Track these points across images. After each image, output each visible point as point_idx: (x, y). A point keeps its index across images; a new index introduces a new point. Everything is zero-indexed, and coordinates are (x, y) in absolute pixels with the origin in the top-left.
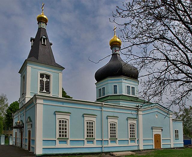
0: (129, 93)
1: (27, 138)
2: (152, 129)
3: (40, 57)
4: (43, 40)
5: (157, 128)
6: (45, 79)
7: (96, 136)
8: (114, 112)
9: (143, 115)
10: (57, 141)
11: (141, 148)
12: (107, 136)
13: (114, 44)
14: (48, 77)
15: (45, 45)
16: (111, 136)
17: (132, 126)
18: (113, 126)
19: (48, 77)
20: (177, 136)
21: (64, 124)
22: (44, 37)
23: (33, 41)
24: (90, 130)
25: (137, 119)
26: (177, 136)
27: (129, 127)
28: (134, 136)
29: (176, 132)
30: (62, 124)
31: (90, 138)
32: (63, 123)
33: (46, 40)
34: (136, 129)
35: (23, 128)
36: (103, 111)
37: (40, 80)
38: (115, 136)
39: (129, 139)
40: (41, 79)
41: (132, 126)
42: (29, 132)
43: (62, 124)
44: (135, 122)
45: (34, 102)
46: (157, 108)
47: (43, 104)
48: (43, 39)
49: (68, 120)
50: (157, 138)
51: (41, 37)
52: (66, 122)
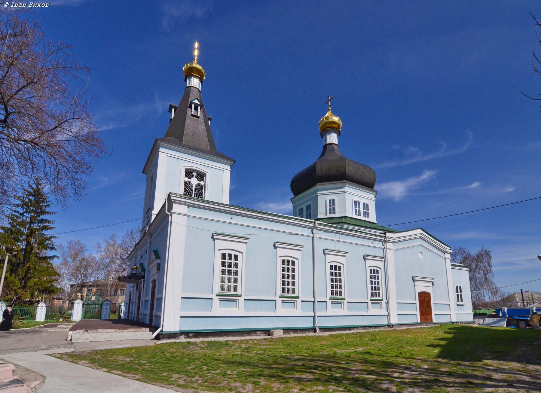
0: (357, 212)
1: (149, 298)
2: (414, 281)
3: (186, 140)
4: (193, 107)
5: (424, 280)
6: (194, 181)
7: (302, 288)
8: (339, 241)
9: (394, 250)
10: (216, 300)
11: (394, 320)
12: (324, 291)
13: (328, 126)
14: (201, 176)
15: (198, 117)
16: (332, 293)
17: (374, 272)
18: (336, 269)
19: (201, 176)
20: (459, 298)
21: (233, 261)
22: (196, 101)
23: (173, 110)
24: (288, 278)
25: (383, 258)
26: (459, 298)
27: (369, 274)
28: (379, 293)
29: (459, 289)
30: (227, 261)
31: (288, 293)
32: (230, 259)
33: (199, 107)
34: (382, 280)
35: (143, 280)
36: (317, 238)
37: (185, 182)
38: (341, 292)
39: (368, 301)
40: (187, 179)
41: (374, 272)
42: (154, 282)
43: (227, 261)
44: (380, 264)
45: (166, 211)
46: (421, 238)
47: (188, 216)
48: (193, 105)
49: (242, 253)
50: (425, 300)
51: (190, 102)
52: (236, 257)
